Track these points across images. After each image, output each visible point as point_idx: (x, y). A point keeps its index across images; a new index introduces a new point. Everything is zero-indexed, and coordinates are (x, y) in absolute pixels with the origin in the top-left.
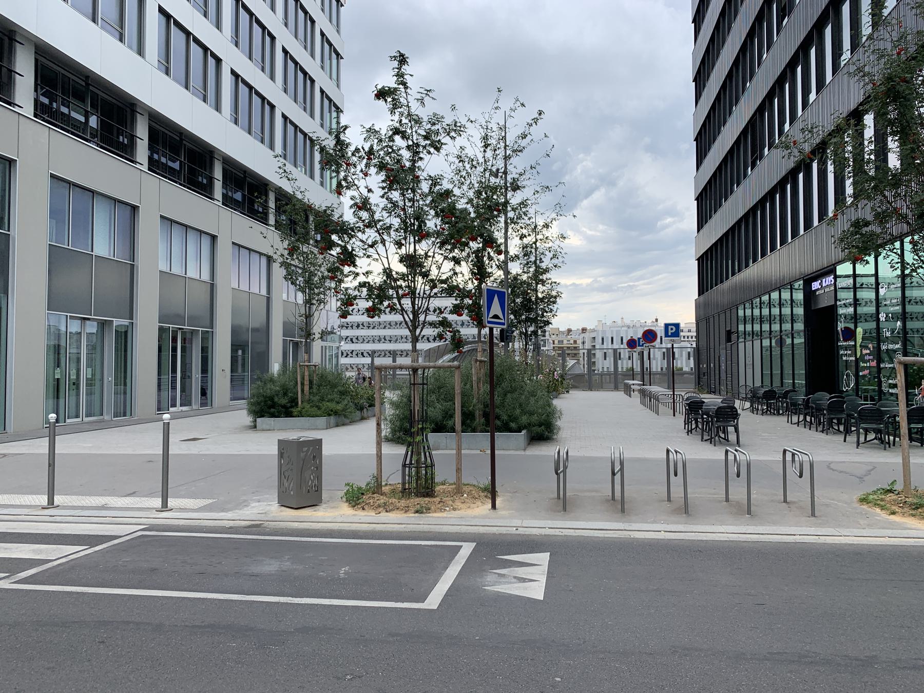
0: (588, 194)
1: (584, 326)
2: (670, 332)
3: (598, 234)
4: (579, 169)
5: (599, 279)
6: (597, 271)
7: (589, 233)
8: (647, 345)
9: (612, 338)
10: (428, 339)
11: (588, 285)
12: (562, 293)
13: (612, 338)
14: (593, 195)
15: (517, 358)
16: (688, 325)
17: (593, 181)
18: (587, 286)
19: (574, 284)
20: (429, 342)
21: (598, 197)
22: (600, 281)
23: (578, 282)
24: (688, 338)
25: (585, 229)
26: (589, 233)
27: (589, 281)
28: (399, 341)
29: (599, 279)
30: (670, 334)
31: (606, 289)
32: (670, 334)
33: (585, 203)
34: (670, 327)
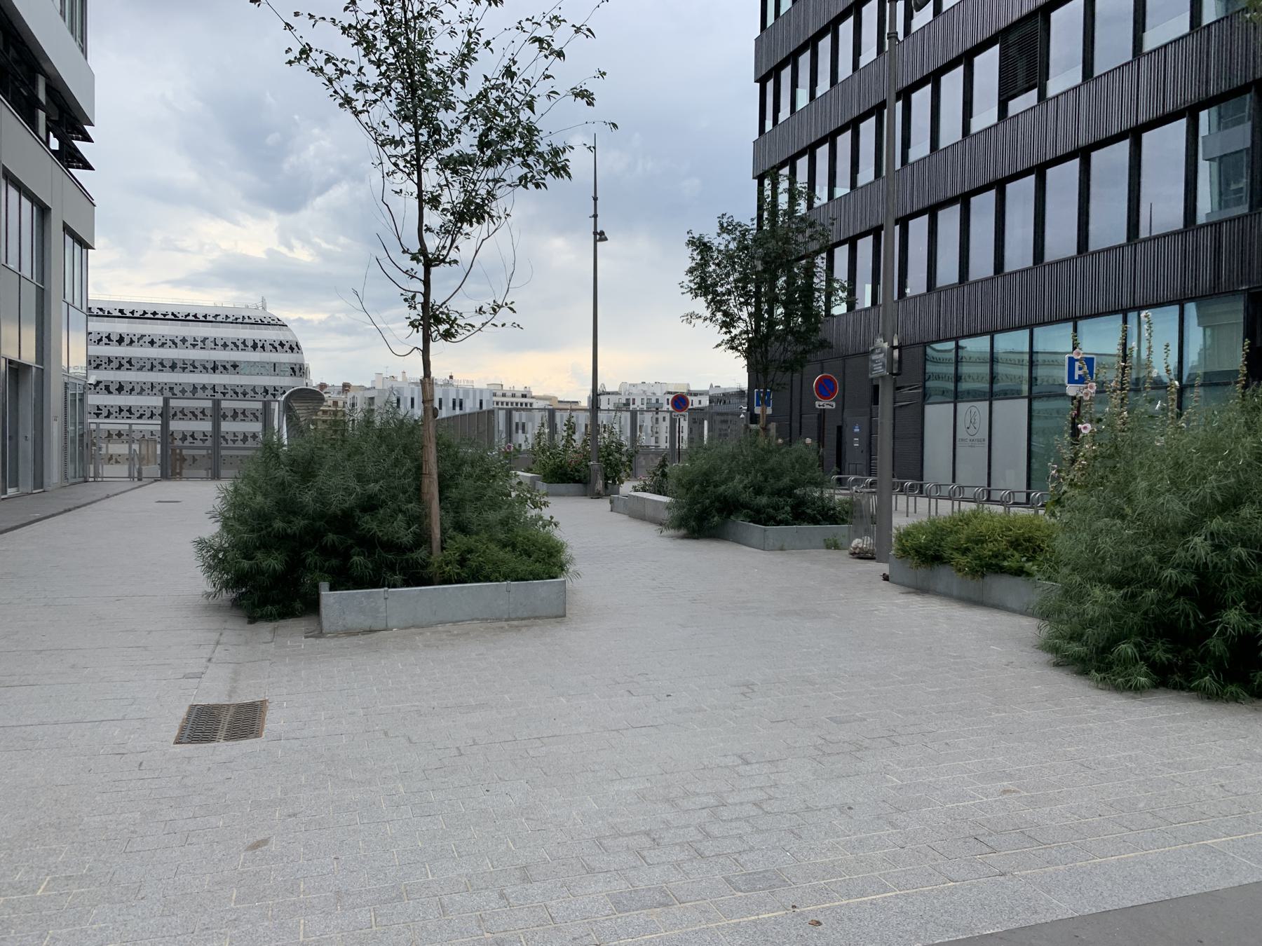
0: (325, 188)
1: (346, 381)
2: (1077, 373)
3: (340, 250)
4: (312, 148)
5: (337, 315)
6: (338, 304)
7: (325, 245)
8: (677, 413)
9: (412, 400)
10: (107, 388)
11: (321, 322)
12: (702, 247)
13: (412, 400)
14: (331, 192)
15: (1233, 480)
16: (492, 387)
17: (332, 171)
18: (320, 323)
19: (300, 320)
20: (110, 392)
21: (339, 194)
22: (340, 318)
23: (306, 317)
24: (507, 404)
25: (317, 240)
26: (325, 245)
27: (323, 316)
28: (104, 366)
29: (337, 315)
30: (1076, 378)
31: (347, 330)
32: (1076, 378)
33: (319, 201)
34: (1077, 364)
